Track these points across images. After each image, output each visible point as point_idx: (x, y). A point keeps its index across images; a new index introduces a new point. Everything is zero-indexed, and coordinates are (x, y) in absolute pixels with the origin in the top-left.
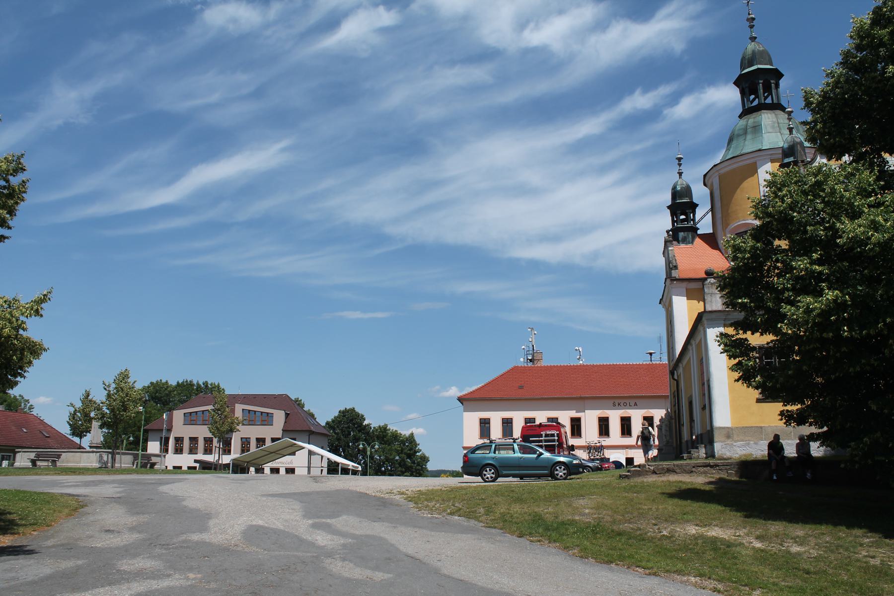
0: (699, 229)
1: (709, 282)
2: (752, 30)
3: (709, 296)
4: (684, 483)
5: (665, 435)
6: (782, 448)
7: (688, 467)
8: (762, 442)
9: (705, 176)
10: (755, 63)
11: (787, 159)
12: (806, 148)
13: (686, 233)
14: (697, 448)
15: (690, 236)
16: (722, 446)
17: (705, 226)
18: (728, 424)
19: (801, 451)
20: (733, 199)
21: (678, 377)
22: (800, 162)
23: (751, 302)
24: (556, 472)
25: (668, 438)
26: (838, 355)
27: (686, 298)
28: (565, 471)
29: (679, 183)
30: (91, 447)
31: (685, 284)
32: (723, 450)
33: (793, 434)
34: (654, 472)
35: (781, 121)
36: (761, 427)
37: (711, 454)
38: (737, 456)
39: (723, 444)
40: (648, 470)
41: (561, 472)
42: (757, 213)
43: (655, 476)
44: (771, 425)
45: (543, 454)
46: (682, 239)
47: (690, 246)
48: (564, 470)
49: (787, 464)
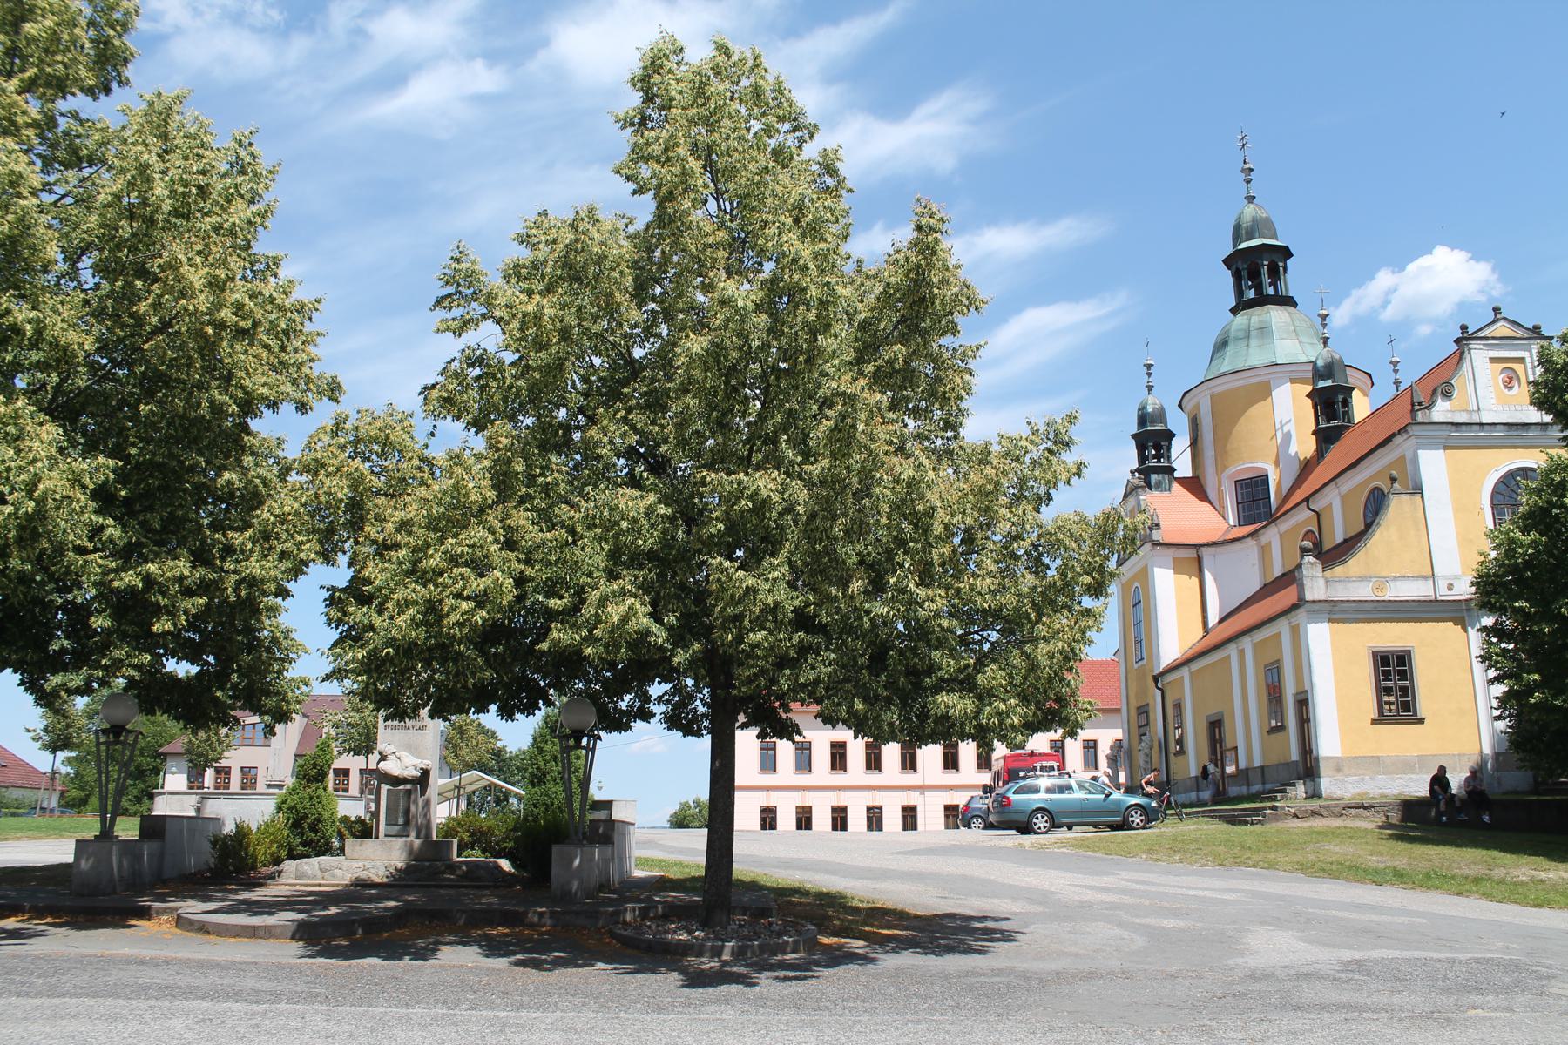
4: (681, 864)
6: (1448, 785)
9: (1186, 393)
17: (1183, 467)
27: (1171, 571)
30: (269, 786)
31: (1171, 551)
34: (1296, 816)
35: (1297, 323)
36: (1378, 757)
37: (1315, 794)
41: (1137, 819)
43: (1296, 820)
49: (1458, 804)
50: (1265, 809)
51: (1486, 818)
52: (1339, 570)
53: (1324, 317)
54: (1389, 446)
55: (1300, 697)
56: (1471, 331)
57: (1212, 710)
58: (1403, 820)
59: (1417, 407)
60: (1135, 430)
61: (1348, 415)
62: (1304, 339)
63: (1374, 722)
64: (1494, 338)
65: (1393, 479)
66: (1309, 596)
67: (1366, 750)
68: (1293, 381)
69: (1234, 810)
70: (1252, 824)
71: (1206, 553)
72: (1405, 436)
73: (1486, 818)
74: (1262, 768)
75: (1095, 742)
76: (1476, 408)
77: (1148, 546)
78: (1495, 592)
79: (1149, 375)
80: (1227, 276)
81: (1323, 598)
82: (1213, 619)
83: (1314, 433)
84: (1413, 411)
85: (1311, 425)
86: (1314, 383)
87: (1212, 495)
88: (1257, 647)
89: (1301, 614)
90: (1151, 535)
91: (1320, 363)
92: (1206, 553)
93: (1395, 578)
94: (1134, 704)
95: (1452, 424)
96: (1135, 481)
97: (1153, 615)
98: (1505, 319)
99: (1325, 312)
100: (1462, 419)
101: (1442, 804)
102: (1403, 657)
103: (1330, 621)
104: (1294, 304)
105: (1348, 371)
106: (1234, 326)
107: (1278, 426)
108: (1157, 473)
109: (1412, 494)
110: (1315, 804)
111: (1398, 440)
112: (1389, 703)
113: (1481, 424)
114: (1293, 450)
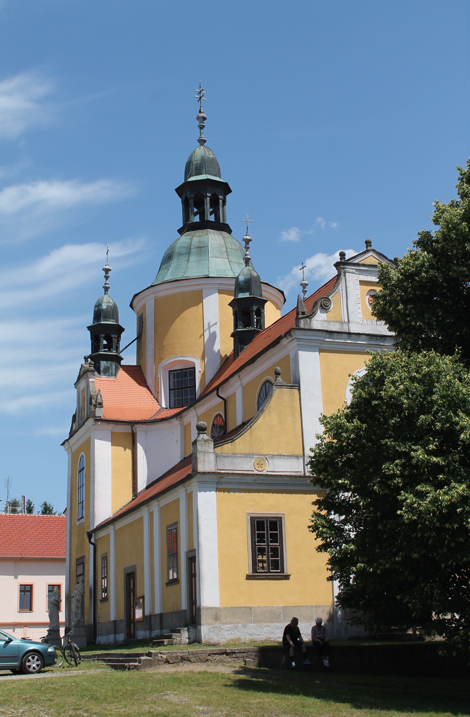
0: (123, 359)
1: (203, 439)
2: (202, 130)
3: (202, 454)
5: (76, 613)
6: (299, 634)
7: (203, 655)
8: (251, 624)
9: (136, 296)
10: (204, 171)
11: (242, 294)
12: (262, 285)
13: (109, 362)
14: (179, 631)
15: (114, 367)
16: (209, 629)
18: (217, 604)
19: (318, 636)
20: (171, 329)
21: (95, 540)
22: (301, 313)
23: (351, 484)
24: (28, 664)
25: (79, 616)
26: (453, 544)
28: (39, 662)
29: (105, 300)
31: (110, 427)
32: (211, 634)
33: (282, 615)
34: (167, 662)
35: (229, 246)
36: (250, 608)
38: (225, 641)
39: (210, 626)
40: (160, 658)
41: (34, 664)
42: (361, 393)
43: (167, 666)
44: (261, 606)
45: (12, 641)
46: (104, 369)
47: (112, 378)
48: (37, 660)
49: (304, 650)
50: (142, 655)
51: (326, 662)
52: (227, 448)
53: (247, 241)
54: (278, 347)
55: (191, 555)
56: (347, 257)
57: (128, 563)
58: (259, 665)
59: (301, 316)
60: (91, 323)
61: (260, 323)
62: (233, 259)
63: (249, 577)
64: (364, 265)
65: (277, 374)
66: (201, 468)
67: (242, 602)
68: (221, 292)
69: (122, 655)
70: (129, 669)
71: (139, 429)
72: (290, 339)
73: (326, 662)
74: (161, 615)
75: (31, 586)
76: (346, 320)
77: (91, 421)
78: (325, 470)
79: (107, 278)
80: (178, 202)
81: (213, 470)
82: (142, 485)
83: (233, 335)
84: (298, 319)
85: (231, 329)
86: (235, 295)
87: (150, 382)
88: (163, 510)
89: (194, 481)
90: (94, 412)
91: (241, 278)
92: (139, 429)
93: (273, 456)
94: (75, 556)
95: (327, 331)
96: (87, 366)
97: (92, 479)
98: (374, 251)
99: (248, 237)
100: (335, 327)
101: (292, 653)
102: (276, 523)
103: (218, 490)
104: (229, 231)
105: (264, 287)
106: (179, 244)
107: (206, 327)
108: (107, 360)
109: (292, 387)
110: (195, 648)
111: (284, 341)
112: (263, 561)
113: (349, 334)
114: (217, 347)
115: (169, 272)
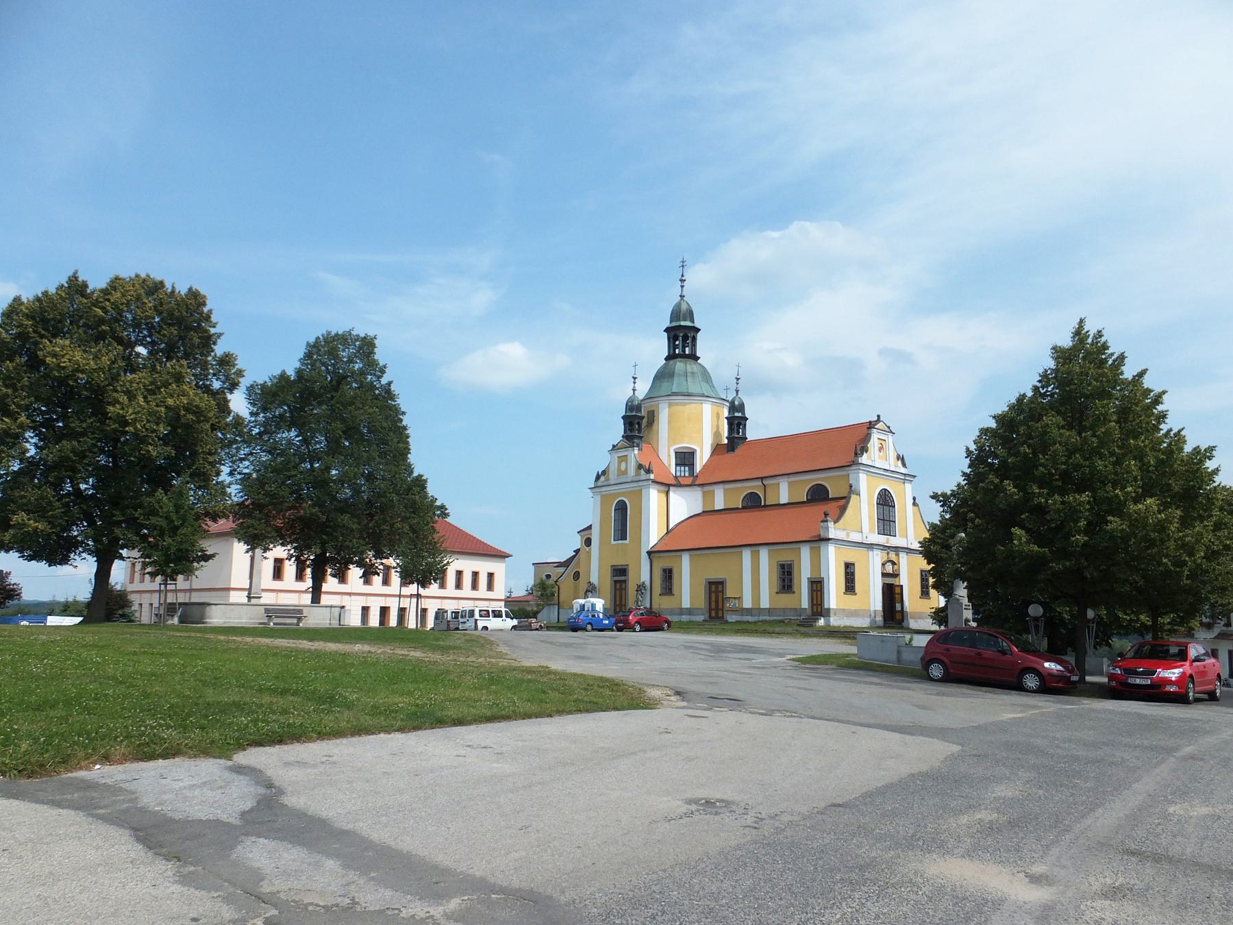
115: (674, 385)
